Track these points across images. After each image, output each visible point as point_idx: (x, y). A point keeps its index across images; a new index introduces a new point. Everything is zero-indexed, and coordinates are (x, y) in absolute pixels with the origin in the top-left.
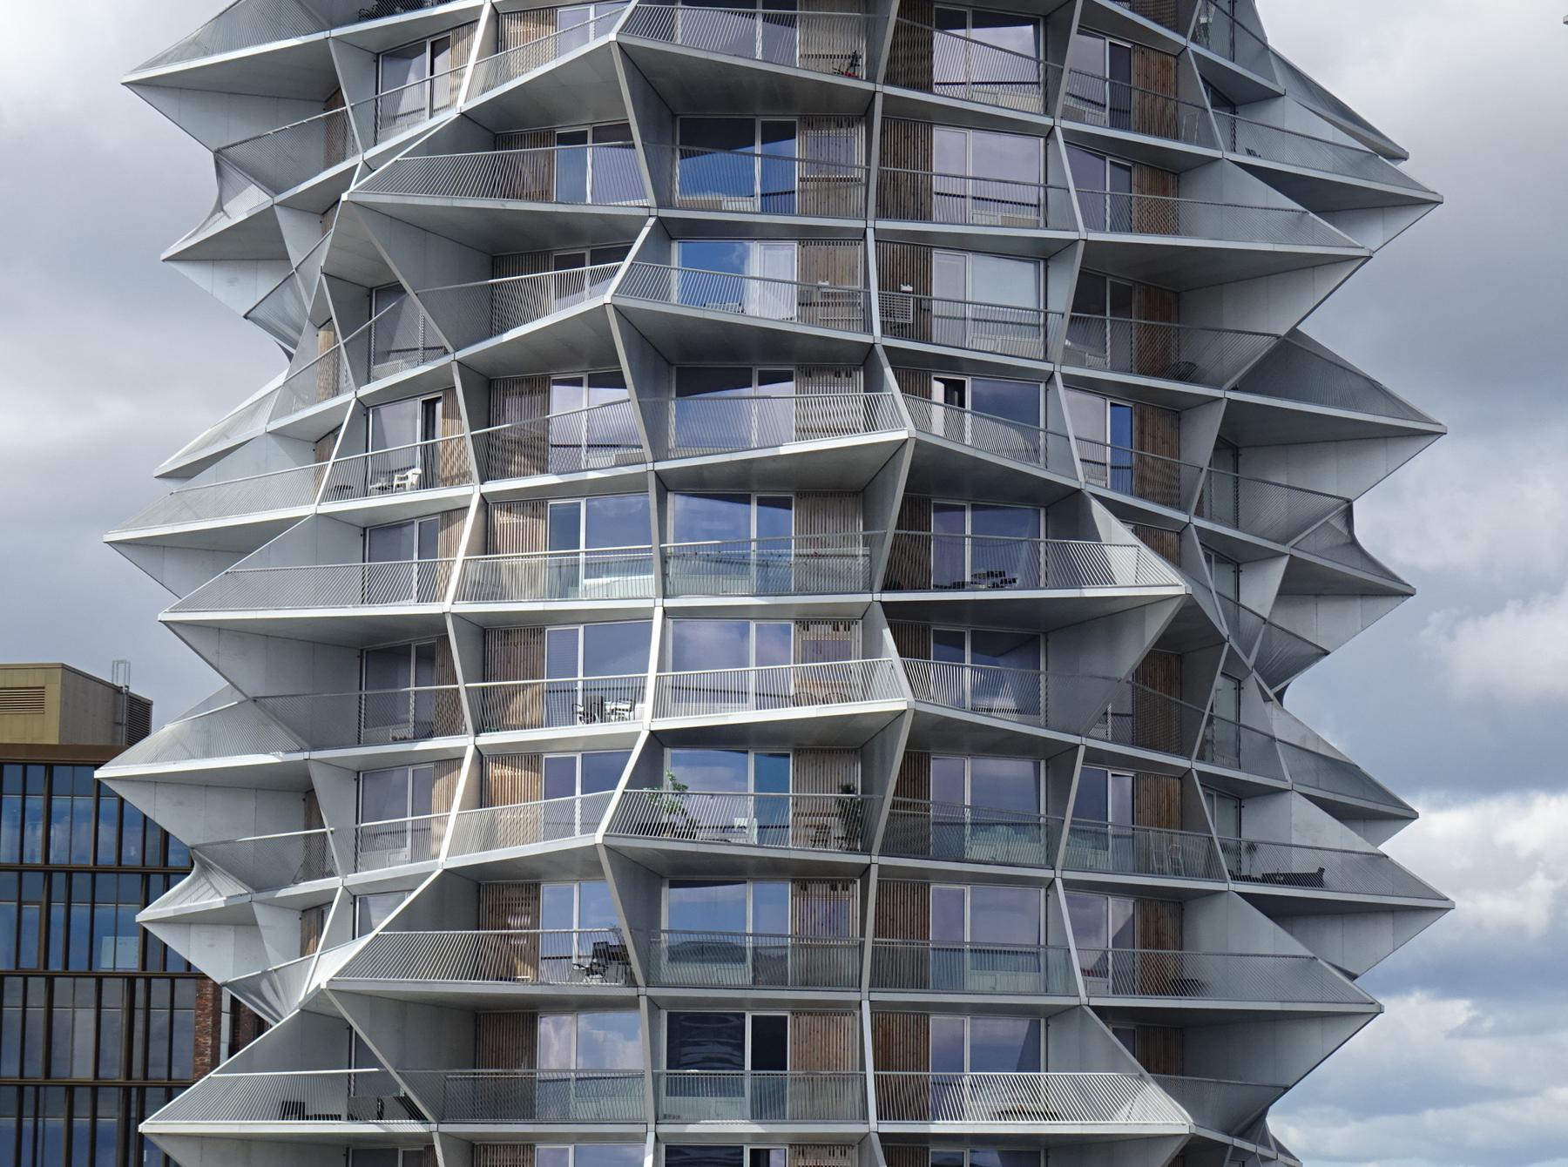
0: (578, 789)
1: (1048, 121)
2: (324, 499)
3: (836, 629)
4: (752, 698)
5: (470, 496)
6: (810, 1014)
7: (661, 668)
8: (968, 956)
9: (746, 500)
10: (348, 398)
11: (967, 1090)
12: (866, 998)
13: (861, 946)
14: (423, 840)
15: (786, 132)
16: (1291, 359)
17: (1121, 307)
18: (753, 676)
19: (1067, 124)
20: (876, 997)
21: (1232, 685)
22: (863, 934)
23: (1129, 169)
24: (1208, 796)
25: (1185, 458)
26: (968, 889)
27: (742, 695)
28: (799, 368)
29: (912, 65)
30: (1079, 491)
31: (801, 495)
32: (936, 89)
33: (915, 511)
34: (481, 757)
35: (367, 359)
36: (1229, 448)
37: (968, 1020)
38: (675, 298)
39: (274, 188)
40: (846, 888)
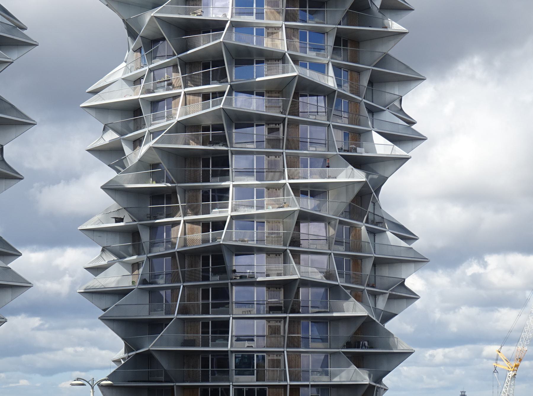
0: (211, 230)
1: (328, 123)
2: (141, 94)
3: (276, 157)
4: (255, 207)
5: (181, 92)
6: (271, 172)
7: (232, 200)
8: (309, 143)
9: (252, 126)
10: (147, 68)
11: (310, 374)
12: (285, 350)
13: (284, 337)
14: (170, 116)
15: (262, 62)
16: (385, 60)
17: (345, 45)
18: (255, 202)
19: (333, 123)
20: (288, 350)
21: (372, 204)
22: (283, 135)
23: (347, 71)
24: (369, 295)
25: (361, 84)
26: (310, 355)
27: (252, 207)
28: (266, 123)
29: (295, 111)
30: (338, 285)
31: (268, 92)
32: (300, 114)
33: (297, 95)
34: (185, 94)
35: (153, 57)
36: (371, 83)
37: (309, 127)
38: (234, 40)
39: (121, 134)
40: (279, 190)
